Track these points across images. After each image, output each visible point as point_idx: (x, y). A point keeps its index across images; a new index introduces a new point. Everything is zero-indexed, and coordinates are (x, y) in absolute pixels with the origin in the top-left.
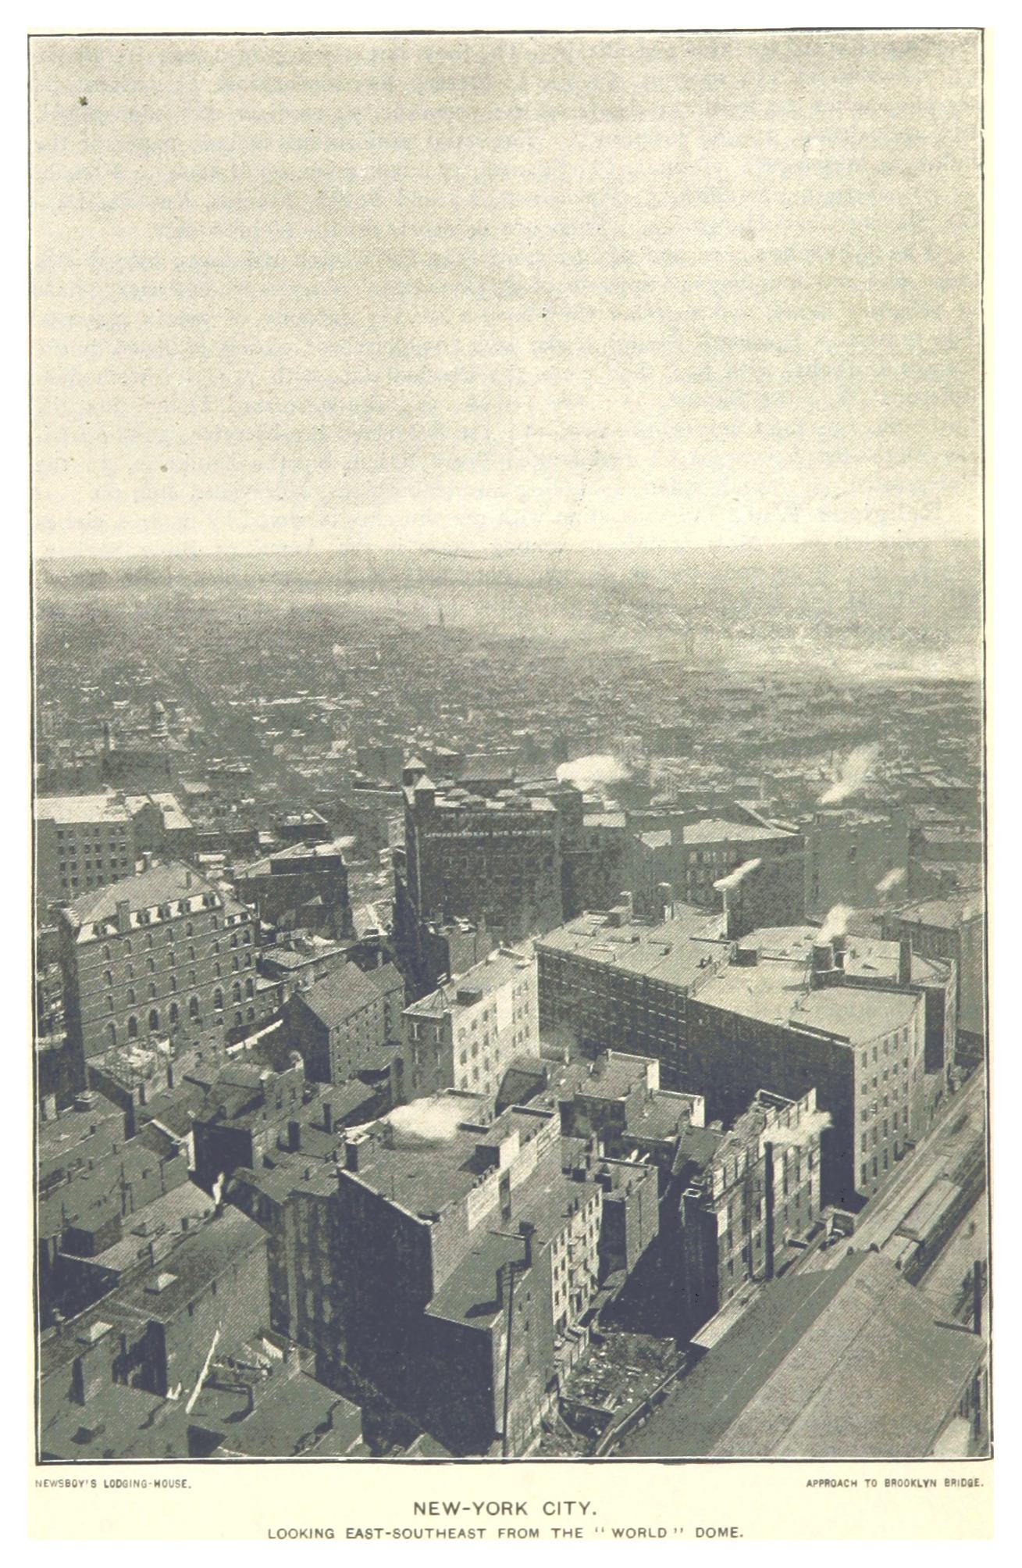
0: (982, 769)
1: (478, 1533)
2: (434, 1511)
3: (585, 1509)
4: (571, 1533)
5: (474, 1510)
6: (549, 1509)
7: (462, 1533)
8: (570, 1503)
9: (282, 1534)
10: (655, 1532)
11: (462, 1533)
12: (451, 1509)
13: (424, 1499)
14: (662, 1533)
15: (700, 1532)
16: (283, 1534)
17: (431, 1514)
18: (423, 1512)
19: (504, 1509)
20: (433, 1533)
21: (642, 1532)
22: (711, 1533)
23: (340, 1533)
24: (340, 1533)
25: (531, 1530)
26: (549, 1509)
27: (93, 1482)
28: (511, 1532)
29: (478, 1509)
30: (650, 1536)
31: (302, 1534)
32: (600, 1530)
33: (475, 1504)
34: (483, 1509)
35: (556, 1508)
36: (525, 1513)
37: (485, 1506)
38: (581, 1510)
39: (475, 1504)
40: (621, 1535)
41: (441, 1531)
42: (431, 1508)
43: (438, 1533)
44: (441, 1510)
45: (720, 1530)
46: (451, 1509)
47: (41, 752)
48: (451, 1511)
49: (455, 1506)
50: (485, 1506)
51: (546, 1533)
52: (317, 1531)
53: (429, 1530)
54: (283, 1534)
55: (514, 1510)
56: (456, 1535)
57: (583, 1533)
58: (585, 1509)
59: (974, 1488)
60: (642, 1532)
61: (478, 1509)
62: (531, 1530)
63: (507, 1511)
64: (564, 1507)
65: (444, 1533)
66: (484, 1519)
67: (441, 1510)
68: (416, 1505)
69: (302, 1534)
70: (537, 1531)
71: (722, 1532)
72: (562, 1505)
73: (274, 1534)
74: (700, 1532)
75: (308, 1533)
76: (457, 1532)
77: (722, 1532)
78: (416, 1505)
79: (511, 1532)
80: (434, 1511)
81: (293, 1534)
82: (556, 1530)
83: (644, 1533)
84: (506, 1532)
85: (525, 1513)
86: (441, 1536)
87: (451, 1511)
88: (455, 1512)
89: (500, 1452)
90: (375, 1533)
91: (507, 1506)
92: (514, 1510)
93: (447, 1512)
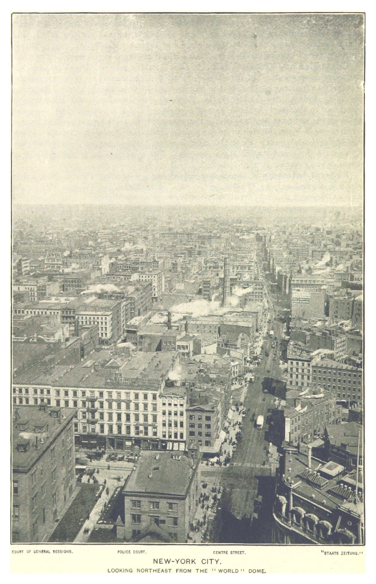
0: (363, 284)
1: (169, 571)
2: (161, 562)
3: (217, 562)
5: (176, 562)
6: (204, 562)
7: (163, 571)
8: (211, 560)
9: (113, 571)
10: (234, 571)
11: (163, 571)
12: (168, 561)
13: (157, 557)
14: (237, 571)
15: (251, 571)
16: (116, 571)
17: (160, 563)
18: (157, 562)
19: (187, 561)
20: (152, 571)
21: (229, 571)
22: (254, 571)
23: (135, 570)
24: (135, 570)
25: (188, 570)
26: (204, 562)
27: (337, 553)
28: (181, 571)
29: (177, 562)
30: (232, 572)
32: (214, 570)
34: (179, 562)
36: (195, 563)
37: (180, 561)
38: (176, 562)
41: (202, 570)
42: (160, 561)
44: (163, 562)
45: (258, 570)
46: (168, 561)
47: (361, 38)
48: (167, 562)
50: (180, 561)
51: (194, 571)
52: (126, 569)
53: (150, 569)
54: (116, 571)
55: (191, 562)
56: (161, 571)
57: (208, 571)
58: (217, 562)
59: (43, 550)
60: (229, 571)
61: (177, 562)
63: (188, 562)
64: (209, 561)
67: (163, 562)
68: (154, 560)
72: (209, 560)
74: (251, 571)
75: (123, 570)
76: (161, 570)
79: (181, 571)
80: (161, 562)
81: (117, 571)
82: (197, 570)
84: (179, 570)
85: (195, 563)
87: (167, 562)
88: (169, 562)
89: (285, 542)
90: (149, 571)
91: (188, 560)
92: (191, 562)
93: (166, 562)
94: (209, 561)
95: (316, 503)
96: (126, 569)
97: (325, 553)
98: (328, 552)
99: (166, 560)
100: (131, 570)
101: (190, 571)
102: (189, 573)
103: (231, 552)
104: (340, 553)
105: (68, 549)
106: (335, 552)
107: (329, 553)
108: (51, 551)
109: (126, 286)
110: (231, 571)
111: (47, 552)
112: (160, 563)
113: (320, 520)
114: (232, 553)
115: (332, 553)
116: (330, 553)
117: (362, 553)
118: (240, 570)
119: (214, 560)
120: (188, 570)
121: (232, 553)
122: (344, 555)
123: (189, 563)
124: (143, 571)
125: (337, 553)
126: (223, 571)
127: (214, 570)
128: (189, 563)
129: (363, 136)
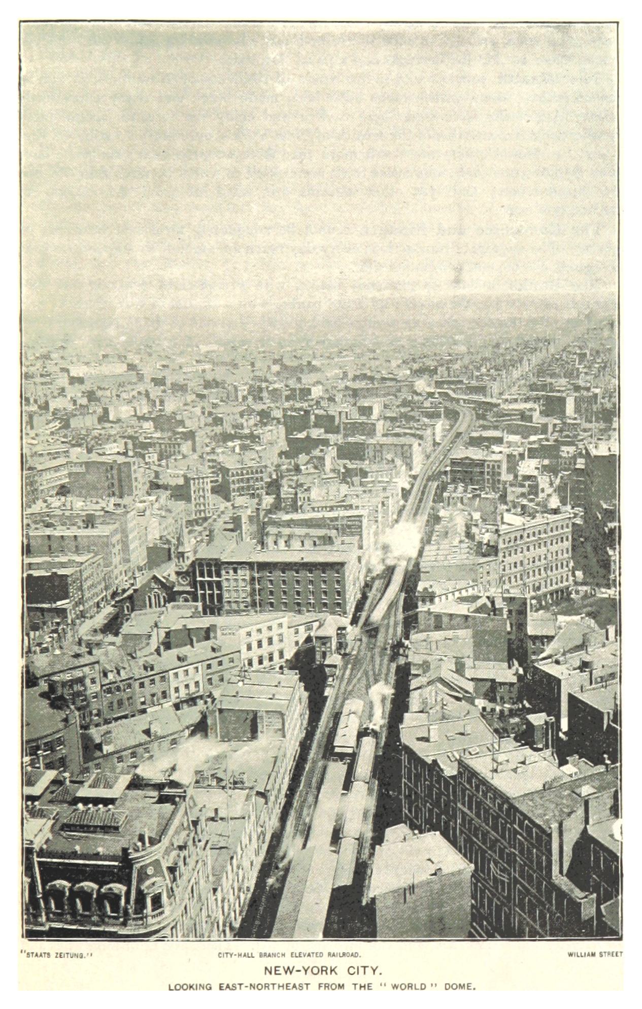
1: (305, 986)
2: (277, 972)
3: (374, 971)
4: (283, 986)
5: (303, 971)
6: (352, 971)
7: (294, 986)
8: (365, 967)
9: (178, 987)
10: (418, 987)
11: (294, 986)
14: (423, 987)
15: (448, 986)
17: (276, 974)
18: (270, 973)
19: (322, 971)
20: (276, 987)
21: (410, 986)
22: (334, 987)
24: (216, 987)
26: (352, 971)
27: (49, 954)
28: (327, 986)
29: (306, 971)
30: (416, 989)
31: (191, 987)
32: (434, 985)
33: (303, 968)
35: (356, 970)
36: (336, 974)
39: (303, 968)
40: (397, 988)
41: (281, 985)
42: (276, 970)
43: (361, 987)
44: (281, 971)
48: (288, 972)
49: (291, 969)
51: (349, 987)
52: (200, 985)
53: (273, 984)
55: (329, 971)
56: (291, 987)
57: (373, 986)
58: (374, 971)
60: (410, 986)
61: (306, 971)
62: (460, 985)
63: (324, 973)
64: (361, 970)
65: (364, 986)
66: (309, 978)
67: (281, 971)
68: (266, 968)
69: (191, 987)
70: (343, 985)
71: (461, 986)
72: (360, 968)
73: (172, 987)
74: (448, 986)
75: (194, 987)
76: (291, 986)
77: (461, 986)
78: (266, 968)
79: (327, 986)
80: (277, 972)
81: (185, 987)
82: (355, 984)
83: (411, 987)
85: (336, 974)
86: (281, 988)
87: (288, 972)
88: (291, 973)
90: (271, 987)
91: (324, 969)
92: (329, 971)
93: (286, 972)
94: (361, 970)
95: (61, 858)
96: (200, 985)
97: (28, 954)
98: (33, 953)
99: (286, 969)
100: (208, 986)
101: (341, 986)
102: (341, 991)
103: (601, 953)
104: (53, 955)
105: (78, 952)
106: (45, 953)
107: (34, 955)
108: (256, 955)
109: (258, 525)
110: (413, 987)
111: (245, 955)
112: (276, 974)
113: (101, 887)
114: (601, 956)
115: (39, 955)
116: (37, 955)
117: (22, 952)
118: (428, 986)
119: (370, 968)
120: (339, 985)
121: (601, 956)
122: (59, 959)
123: (327, 973)
124: (403, 987)
125: (49, 954)
126: (399, 988)
127: (434, 985)
128: (327, 973)
129: (185, 23)
